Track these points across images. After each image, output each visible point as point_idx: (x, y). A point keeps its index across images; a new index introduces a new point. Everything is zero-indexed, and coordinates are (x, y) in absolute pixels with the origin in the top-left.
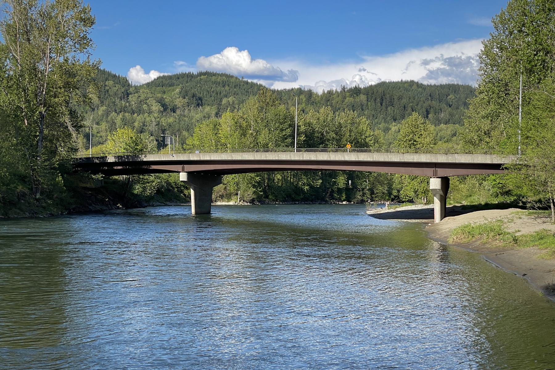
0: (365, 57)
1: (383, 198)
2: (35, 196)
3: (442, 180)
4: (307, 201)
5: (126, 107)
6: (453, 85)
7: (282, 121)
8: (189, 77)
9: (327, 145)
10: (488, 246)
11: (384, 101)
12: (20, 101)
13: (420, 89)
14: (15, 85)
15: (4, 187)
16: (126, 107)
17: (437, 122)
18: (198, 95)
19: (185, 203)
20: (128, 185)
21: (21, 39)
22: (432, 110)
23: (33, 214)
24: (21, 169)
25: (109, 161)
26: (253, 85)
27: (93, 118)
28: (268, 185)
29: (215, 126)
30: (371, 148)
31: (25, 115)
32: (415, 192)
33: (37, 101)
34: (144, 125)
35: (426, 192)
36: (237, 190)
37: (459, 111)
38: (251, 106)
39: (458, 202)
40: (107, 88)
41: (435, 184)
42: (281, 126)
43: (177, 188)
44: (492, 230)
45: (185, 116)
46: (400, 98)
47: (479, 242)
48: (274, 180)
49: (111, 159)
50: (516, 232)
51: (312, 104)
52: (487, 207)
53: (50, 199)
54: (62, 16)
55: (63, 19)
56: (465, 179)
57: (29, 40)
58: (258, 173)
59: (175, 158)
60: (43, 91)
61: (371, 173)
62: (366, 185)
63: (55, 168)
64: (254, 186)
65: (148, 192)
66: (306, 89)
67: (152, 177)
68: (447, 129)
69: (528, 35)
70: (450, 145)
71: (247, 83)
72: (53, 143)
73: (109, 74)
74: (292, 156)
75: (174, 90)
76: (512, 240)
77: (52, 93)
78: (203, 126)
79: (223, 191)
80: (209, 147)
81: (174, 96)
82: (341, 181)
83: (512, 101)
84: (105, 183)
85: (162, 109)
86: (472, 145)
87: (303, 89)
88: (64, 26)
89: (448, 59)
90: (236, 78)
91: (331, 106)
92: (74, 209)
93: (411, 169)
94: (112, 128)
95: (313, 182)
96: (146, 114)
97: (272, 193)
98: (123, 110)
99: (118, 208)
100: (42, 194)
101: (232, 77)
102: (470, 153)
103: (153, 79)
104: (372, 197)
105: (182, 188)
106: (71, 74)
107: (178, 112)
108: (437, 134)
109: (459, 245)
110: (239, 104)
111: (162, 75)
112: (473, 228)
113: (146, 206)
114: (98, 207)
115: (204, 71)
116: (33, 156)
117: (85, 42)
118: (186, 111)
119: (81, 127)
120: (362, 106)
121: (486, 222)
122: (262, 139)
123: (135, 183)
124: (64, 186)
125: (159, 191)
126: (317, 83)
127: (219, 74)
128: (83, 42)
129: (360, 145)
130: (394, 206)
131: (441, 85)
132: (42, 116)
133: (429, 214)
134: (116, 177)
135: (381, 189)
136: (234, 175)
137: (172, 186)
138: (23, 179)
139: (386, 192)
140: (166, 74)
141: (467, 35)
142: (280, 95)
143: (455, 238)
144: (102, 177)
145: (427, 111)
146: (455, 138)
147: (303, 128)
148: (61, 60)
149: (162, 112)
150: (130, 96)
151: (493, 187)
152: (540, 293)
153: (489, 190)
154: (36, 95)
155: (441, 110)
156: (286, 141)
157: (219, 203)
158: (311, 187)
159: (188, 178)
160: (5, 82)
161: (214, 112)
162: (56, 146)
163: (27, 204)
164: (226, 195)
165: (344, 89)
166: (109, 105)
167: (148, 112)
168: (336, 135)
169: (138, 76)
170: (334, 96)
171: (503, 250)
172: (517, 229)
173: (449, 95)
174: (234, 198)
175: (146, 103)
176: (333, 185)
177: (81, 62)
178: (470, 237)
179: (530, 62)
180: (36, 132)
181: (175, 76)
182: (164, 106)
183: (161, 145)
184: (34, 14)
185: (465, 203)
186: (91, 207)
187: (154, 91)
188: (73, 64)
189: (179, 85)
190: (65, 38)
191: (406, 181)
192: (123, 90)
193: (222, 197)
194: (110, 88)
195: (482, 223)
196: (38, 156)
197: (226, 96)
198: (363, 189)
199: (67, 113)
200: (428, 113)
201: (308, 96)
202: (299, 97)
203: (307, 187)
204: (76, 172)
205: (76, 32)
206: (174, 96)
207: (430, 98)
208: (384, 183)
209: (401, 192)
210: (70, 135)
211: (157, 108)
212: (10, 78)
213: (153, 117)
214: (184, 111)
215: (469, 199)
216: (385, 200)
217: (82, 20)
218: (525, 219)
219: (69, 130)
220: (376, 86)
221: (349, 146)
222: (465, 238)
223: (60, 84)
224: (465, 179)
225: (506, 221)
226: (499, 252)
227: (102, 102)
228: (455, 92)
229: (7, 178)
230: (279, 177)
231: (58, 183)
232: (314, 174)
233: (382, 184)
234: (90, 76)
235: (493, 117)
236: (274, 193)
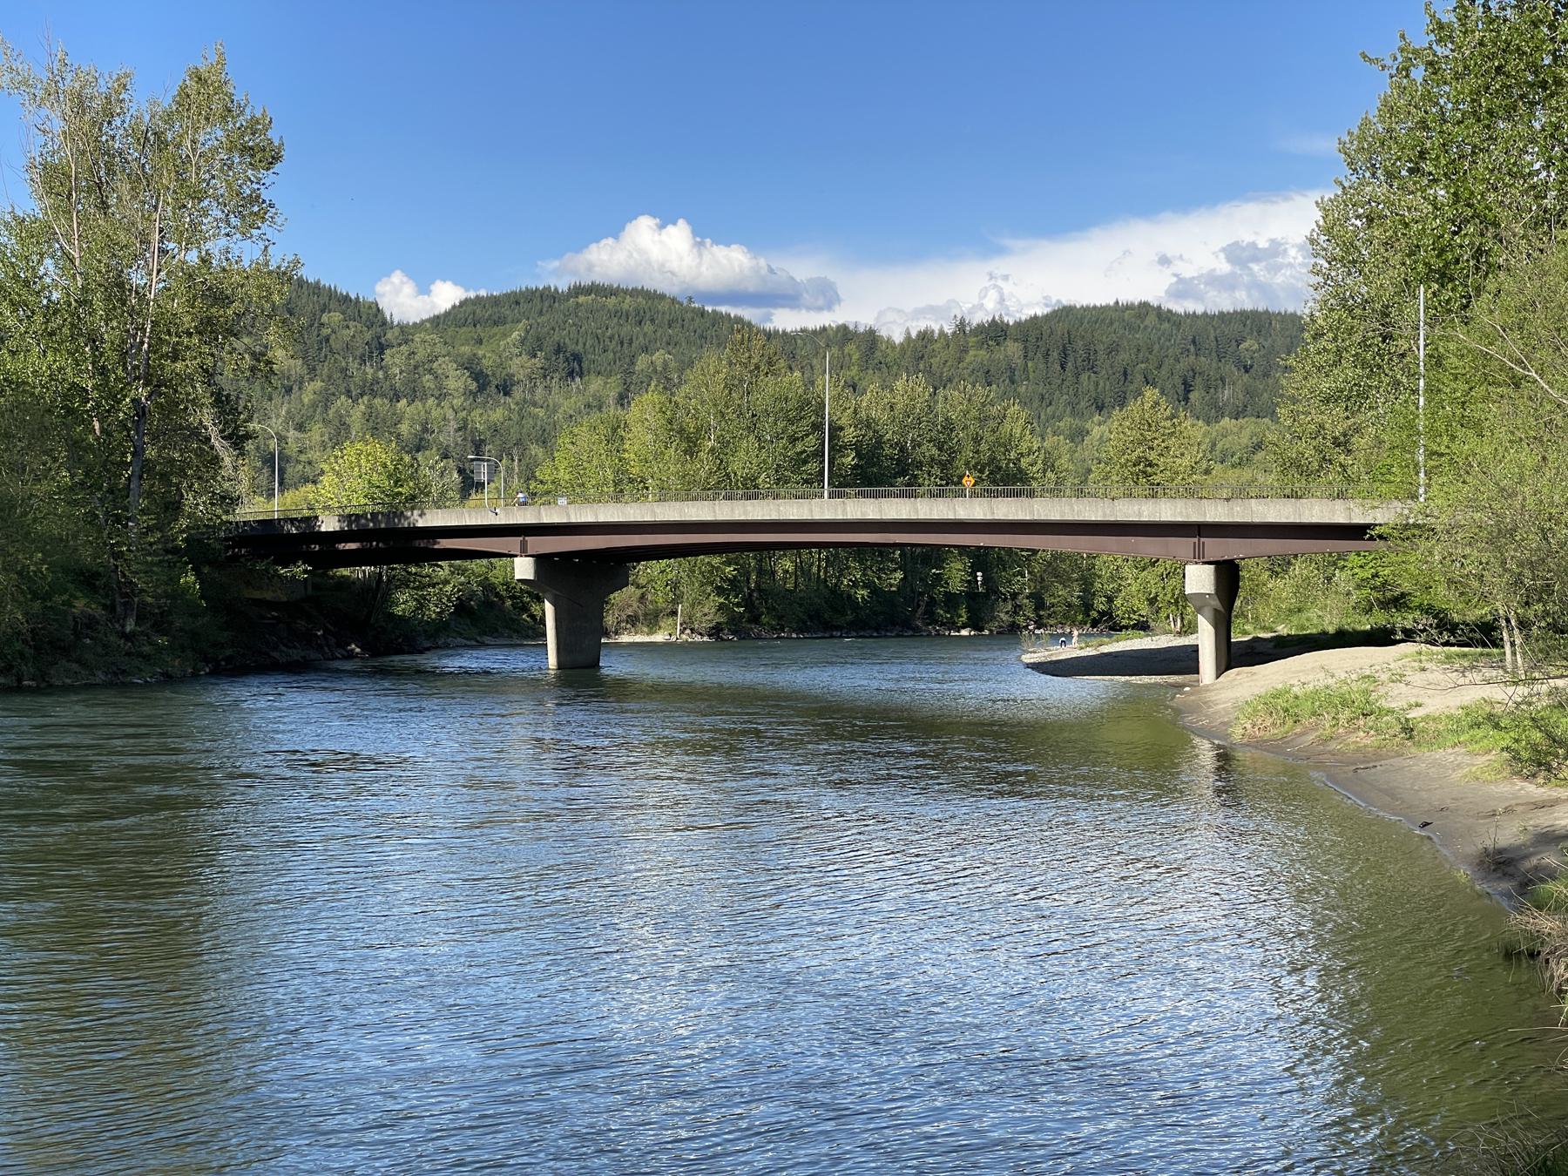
0: (1008, 242)
1: (1068, 619)
2: (123, 626)
3: (1217, 571)
4: (862, 629)
5: (376, 381)
6: (1254, 315)
7: (792, 414)
8: (548, 297)
9: (916, 476)
10: (1333, 746)
11: (1071, 359)
12: (81, 371)
13: (1166, 325)
14: (68, 326)
15: (37, 604)
16: (376, 381)
17: (1214, 412)
18: (571, 347)
19: (533, 639)
20: (376, 593)
21: (87, 204)
22: (1198, 380)
23: (115, 674)
24: (86, 556)
25: (323, 529)
26: (718, 318)
27: (288, 412)
28: (758, 588)
29: (614, 430)
30: (1035, 484)
31: (93, 408)
32: (1152, 601)
33: (125, 369)
34: (425, 430)
35: (1181, 600)
36: (675, 602)
37: (1271, 381)
38: (711, 371)
39: (1264, 628)
40: (326, 331)
41: (1200, 579)
42: (791, 429)
43: (513, 597)
44: (1344, 704)
45: (535, 404)
46: (1113, 350)
47: (1311, 737)
48: (773, 573)
49: (329, 524)
50: (1411, 707)
51: (878, 366)
52: (1343, 639)
53: (164, 633)
54: (194, 142)
55: (194, 150)
56: (1289, 563)
57: (104, 206)
58: (731, 556)
59: (502, 519)
60: (142, 343)
61: (1035, 552)
62: (1023, 583)
63: (176, 551)
64: (720, 591)
65: (433, 611)
66: (861, 330)
67: (444, 569)
68: (1237, 432)
69: (1435, 181)
70: (1247, 474)
71: (703, 313)
72: (170, 484)
73: (331, 294)
74: (1067, 509)
75: (505, 336)
76: (1398, 728)
77: (165, 349)
78: (582, 432)
79: (635, 605)
80: (596, 486)
81: (507, 351)
82: (956, 575)
83: (1403, 355)
84: (316, 587)
85: (474, 386)
86: (1299, 475)
87: (851, 327)
88: (199, 168)
89: (1240, 245)
90: (673, 300)
91: (929, 372)
92: (229, 659)
93: (1133, 539)
94: (340, 434)
95: (879, 578)
96: (431, 401)
97: (771, 609)
98: (370, 389)
99: (351, 656)
100: (140, 619)
101: (662, 297)
102: (1294, 495)
103: (448, 306)
104: (1040, 617)
105: (526, 599)
106: (219, 298)
107: (518, 393)
108: (1214, 445)
109: (1259, 744)
110: (681, 371)
111: (472, 295)
112: (1296, 697)
113: (428, 649)
114: (296, 654)
115: (586, 281)
116: (118, 519)
117: (256, 209)
118: (539, 391)
119: (248, 436)
120: (1013, 371)
121: (1330, 681)
122: (738, 465)
123: (397, 587)
124: (202, 597)
125: (462, 608)
126: (881, 314)
127: (626, 292)
128: (251, 211)
129: (1005, 477)
130: (1095, 641)
131: (1222, 315)
132: (141, 411)
133: (1185, 661)
134: (345, 572)
135: (1064, 594)
136: (664, 562)
137: (497, 595)
138: (88, 580)
139: (1076, 602)
140: (483, 293)
141: (1271, 181)
142: (793, 348)
143: (1249, 726)
144: (305, 571)
145: (1185, 383)
146: (1260, 455)
147: (849, 435)
148: (193, 257)
149: (474, 395)
150: (387, 352)
151: (1359, 587)
152: (1463, 874)
153: (1349, 594)
154: (124, 355)
155: (1222, 379)
156: (798, 473)
157: (625, 638)
158: (875, 591)
159: (537, 572)
160: (39, 319)
161: (613, 394)
162: (178, 489)
163: (100, 650)
164: (645, 615)
165: (962, 325)
166: (330, 377)
167: (437, 393)
168: (940, 449)
169: (407, 300)
170: (937, 346)
171: (1378, 755)
172: (1413, 701)
173: (1243, 339)
174: (666, 622)
175: (430, 371)
176: (934, 586)
177: (246, 263)
178: (1290, 722)
179: (1442, 252)
180: (124, 454)
181: (507, 296)
182: (480, 378)
183: (469, 485)
184: (118, 136)
185: (1283, 630)
186: (275, 654)
187: (453, 338)
188: (224, 270)
189: (519, 321)
190: (200, 200)
191: (1128, 572)
192: (368, 336)
193: (633, 621)
194: (333, 332)
195: (1322, 684)
196: (129, 519)
197: (645, 349)
198: (1014, 596)
199: (207, 401)
200: (1188, 388)
201: (862, 350)
202: (841, 348)
203: (865, 592)
204: (236, 558)
205: (229, 185)
206: (507, 351)
207: (1192, 348)
208: (1069, 579)
209: (1118, 602)
210: (216, 460)
211: (460, 384)
212: (52, 311)
213: (447, 410)
214: (532, 391)
215: (1295, 619)
216: (1073, 624)
217: (246, 150)
218: (1436, 675)
219: (212, 448)
220: (1047, 317)
221: (968, 481)
222: (1273, 724)
223: (188, 322)
224: (1289, 563)
225: (1384, 677)
226: (1365, 760)
227: (312, 370)
228: (1259, 332)
229: (44, 577)
230: (789, 565)
231: (188, 587)
232: (881, 554)
233: (1065, 581)
234: (268, 298)
235: (1353, 398)
236: (774, 609)
